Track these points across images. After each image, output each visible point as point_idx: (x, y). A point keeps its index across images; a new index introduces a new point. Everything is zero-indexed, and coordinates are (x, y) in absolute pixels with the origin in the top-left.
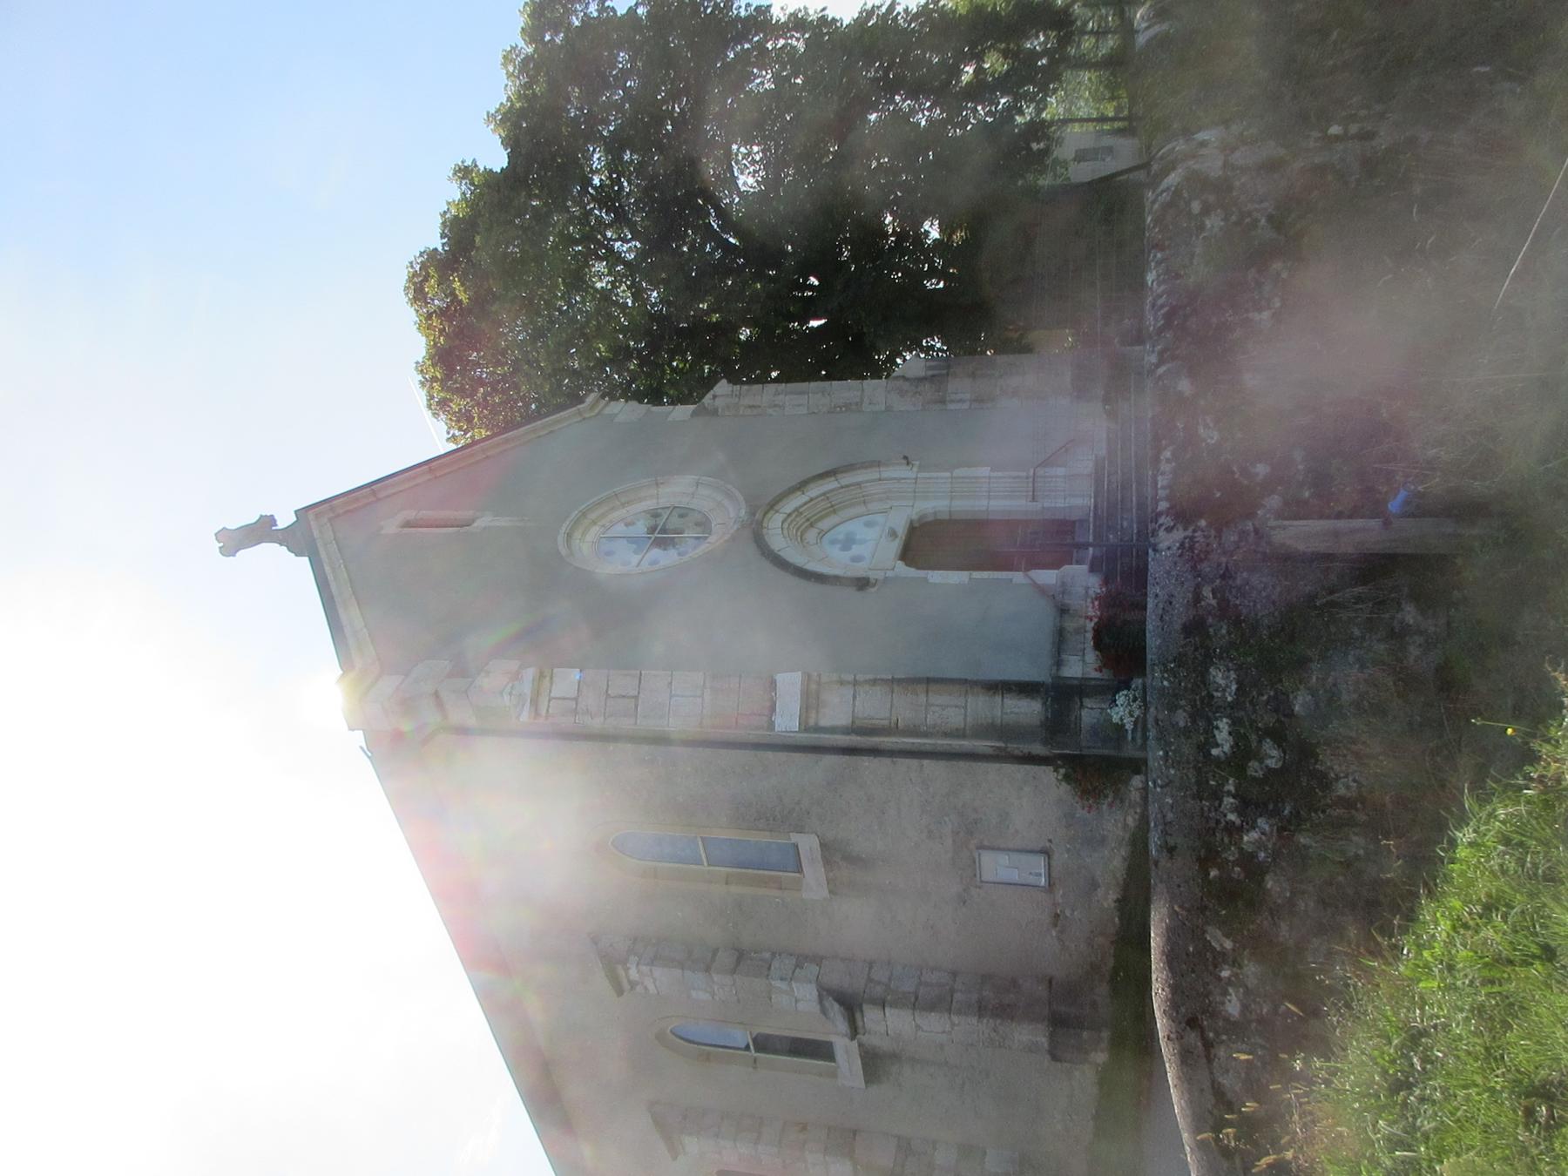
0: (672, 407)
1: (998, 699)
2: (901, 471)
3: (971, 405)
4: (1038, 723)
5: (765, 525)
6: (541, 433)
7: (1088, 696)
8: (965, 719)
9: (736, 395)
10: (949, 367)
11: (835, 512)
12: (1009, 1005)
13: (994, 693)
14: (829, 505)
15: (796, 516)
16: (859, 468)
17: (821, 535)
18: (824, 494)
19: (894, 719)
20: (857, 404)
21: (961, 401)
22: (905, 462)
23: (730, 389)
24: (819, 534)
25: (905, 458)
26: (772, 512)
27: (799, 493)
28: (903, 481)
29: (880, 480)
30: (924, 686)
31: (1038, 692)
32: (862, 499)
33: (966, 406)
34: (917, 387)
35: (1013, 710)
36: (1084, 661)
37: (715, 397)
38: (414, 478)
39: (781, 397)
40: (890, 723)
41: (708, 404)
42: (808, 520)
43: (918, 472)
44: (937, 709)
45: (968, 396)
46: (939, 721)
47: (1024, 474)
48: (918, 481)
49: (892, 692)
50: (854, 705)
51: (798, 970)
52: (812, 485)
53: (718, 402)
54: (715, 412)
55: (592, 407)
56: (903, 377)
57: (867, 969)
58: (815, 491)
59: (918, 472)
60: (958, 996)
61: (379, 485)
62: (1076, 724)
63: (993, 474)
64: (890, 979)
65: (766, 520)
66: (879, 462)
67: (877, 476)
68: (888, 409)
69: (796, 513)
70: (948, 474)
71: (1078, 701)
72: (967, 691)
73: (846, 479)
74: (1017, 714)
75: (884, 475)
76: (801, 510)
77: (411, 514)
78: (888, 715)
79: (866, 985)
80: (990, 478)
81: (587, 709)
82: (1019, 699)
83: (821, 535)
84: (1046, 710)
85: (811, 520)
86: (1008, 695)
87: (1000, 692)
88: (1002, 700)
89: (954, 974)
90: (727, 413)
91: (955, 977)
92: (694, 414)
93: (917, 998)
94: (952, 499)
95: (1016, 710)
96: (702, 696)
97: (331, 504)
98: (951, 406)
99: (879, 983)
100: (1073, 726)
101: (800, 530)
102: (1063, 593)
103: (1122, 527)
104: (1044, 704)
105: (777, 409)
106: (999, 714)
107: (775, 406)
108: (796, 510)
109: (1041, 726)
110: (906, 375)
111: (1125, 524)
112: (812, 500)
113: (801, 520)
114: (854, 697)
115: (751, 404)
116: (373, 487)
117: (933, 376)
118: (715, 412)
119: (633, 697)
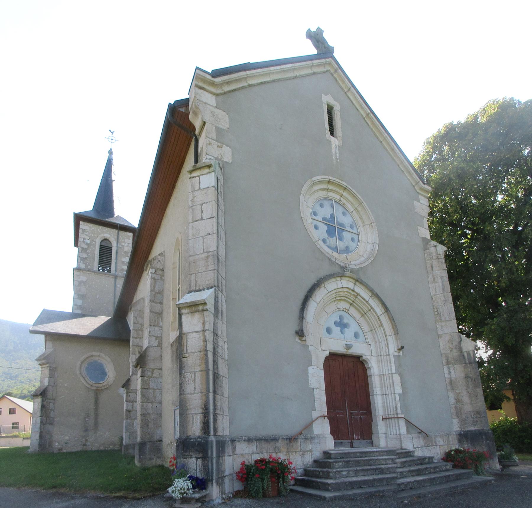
0: (428, 228)
1: (200, 411)
2: (393, 348)
3: (448, 378)
4: (189, 434)
5: (343, 278)
6: (400, 166)
7: (203, 461)
8: (188, 394)
9: (437, 257)
10: (470, 363)
11: (363, 315)
12: (148, 426)
13: (203, 409)
14: (366, 312)
15: (354, 295)
16: (392, 324)
17: (345, 310)
18: (372, 308)
19: (187, 355)
20: (440, 319)
21: (450, 372)
22: (400, 347)
23: (441, 253)
24: (345, 309)
25: (402, 348)
26: (354, 281)
27: (370, 294)
28: (387, 348)
29: (386, 336)
30: (204, 369)
31: (205, 433)
32: (373, 328)
33: (447, 375)
34: (456, 348)
35: (195, 420)
36: (253, 453)
37: (435, 246)
38: (362, 108)
39: (440, 280)
40: (185, 353)
41: (431, 244)
42: (353, 302)
43: (394, 356)
44: (193, 378)
45: (453, 376)
46: (187, 380)
47: (399, 411)
48: (388, 356)
49: (200, 352)
50: (193, 332)
51: (155, 338)
52: (377, 301)
53: (432, 250)
54: (426, 249)
55: (422, 189)
56: (461, 341)
57: (158, 368)
58: (374, 303)
59: (394, 356)
60: (150, 405)
61: (354, 91)
62: (188, 455)
63: (397, 396)
64: (155, 377)
65: (346, 278)
66: (398, 334)
67: (388, 334)
68: (439, 336)
69: (356, 294)
70: (394, 371)
71: (200, 456)
72: (203, 393)
73: (384, 319)
74: (193, 422)
75: (389, 338)
76: (358, 297)
77: (337, 108)
78: (189, 351)
79: (151, 368)
80: (394, 394)
81: (195, 197)
82: (200, 423)
83: (345, 310)
84: (195, 439)
85: (354, 304)
86: (202, 417)
87: (203, 412)
88: (200, 413)
89: (161, 403)
90: (426, 255)
91: (159, 403)
92: (424, 239)
93: (147, 389)
94: (380, 375)
95: (195, 422)
96: (204, 252)
97: (338, 69)
98: (446, 369)
99: (152, 373)
100: (187, 454)
101: (346, 299)
102: (306, 438)
103: (342, 471)
104: (199, 437)
105: (432, 280)
106: (193, 412)
107: (434, 278)
108: (358, 294)
109: (187, 436)
110: (462, 342)
111: (344, 473)
112: (367, 302)
113: (352, 298)
114: (197, 332)
115: (433, 266)
116: (352, 88)
117: (464, 356)
118: (426, 249)
119: (202, 217)
